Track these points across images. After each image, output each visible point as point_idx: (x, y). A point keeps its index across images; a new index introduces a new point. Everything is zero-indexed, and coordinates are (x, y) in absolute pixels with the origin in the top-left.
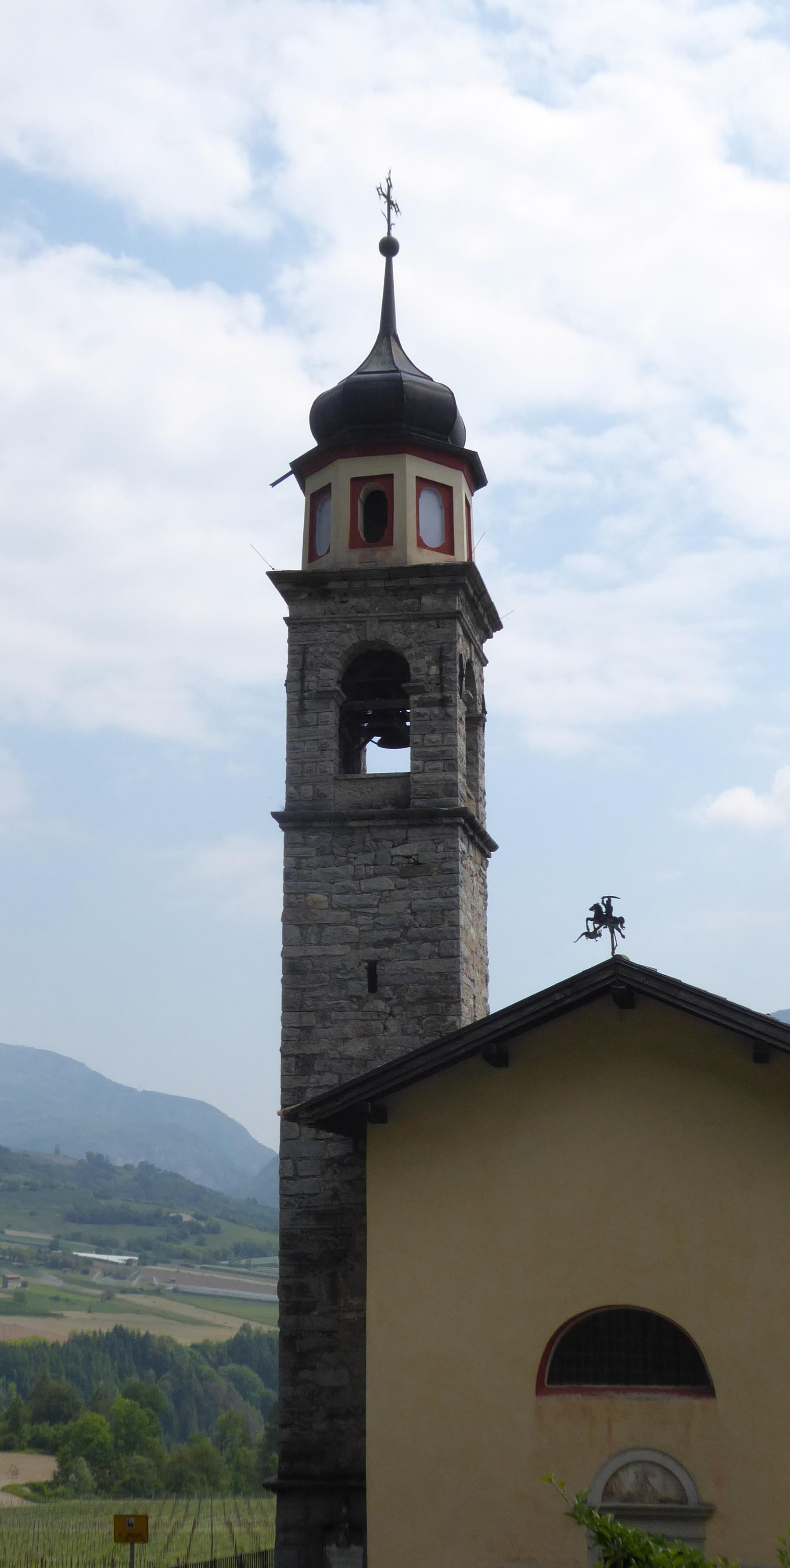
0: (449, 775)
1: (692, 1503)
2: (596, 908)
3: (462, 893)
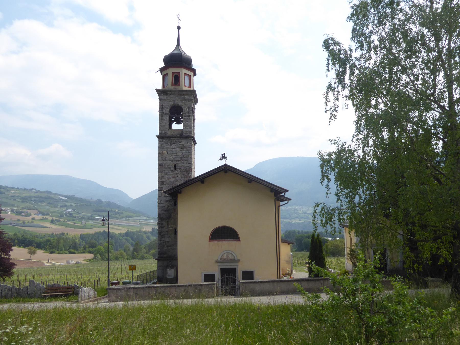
0: (190, 130)
1: (236, 259)
2: (222, 155)
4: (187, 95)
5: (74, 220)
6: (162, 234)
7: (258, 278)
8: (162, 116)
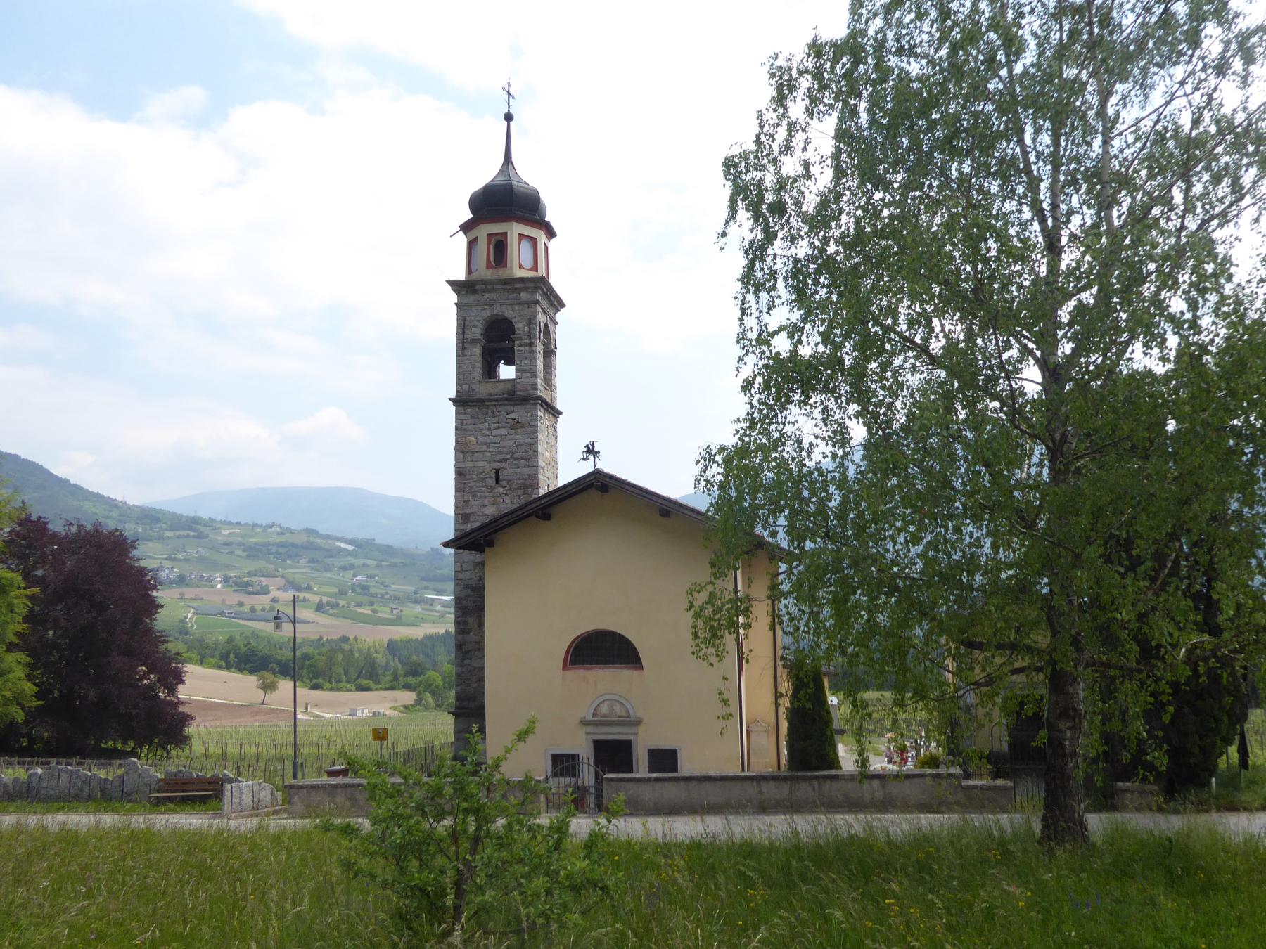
1: (633, 718)
3: (540, 436)
4: (526, 289)
5: (372, 604)
6: (465, 648)
7: (687, 766)
8: (464, 348)
